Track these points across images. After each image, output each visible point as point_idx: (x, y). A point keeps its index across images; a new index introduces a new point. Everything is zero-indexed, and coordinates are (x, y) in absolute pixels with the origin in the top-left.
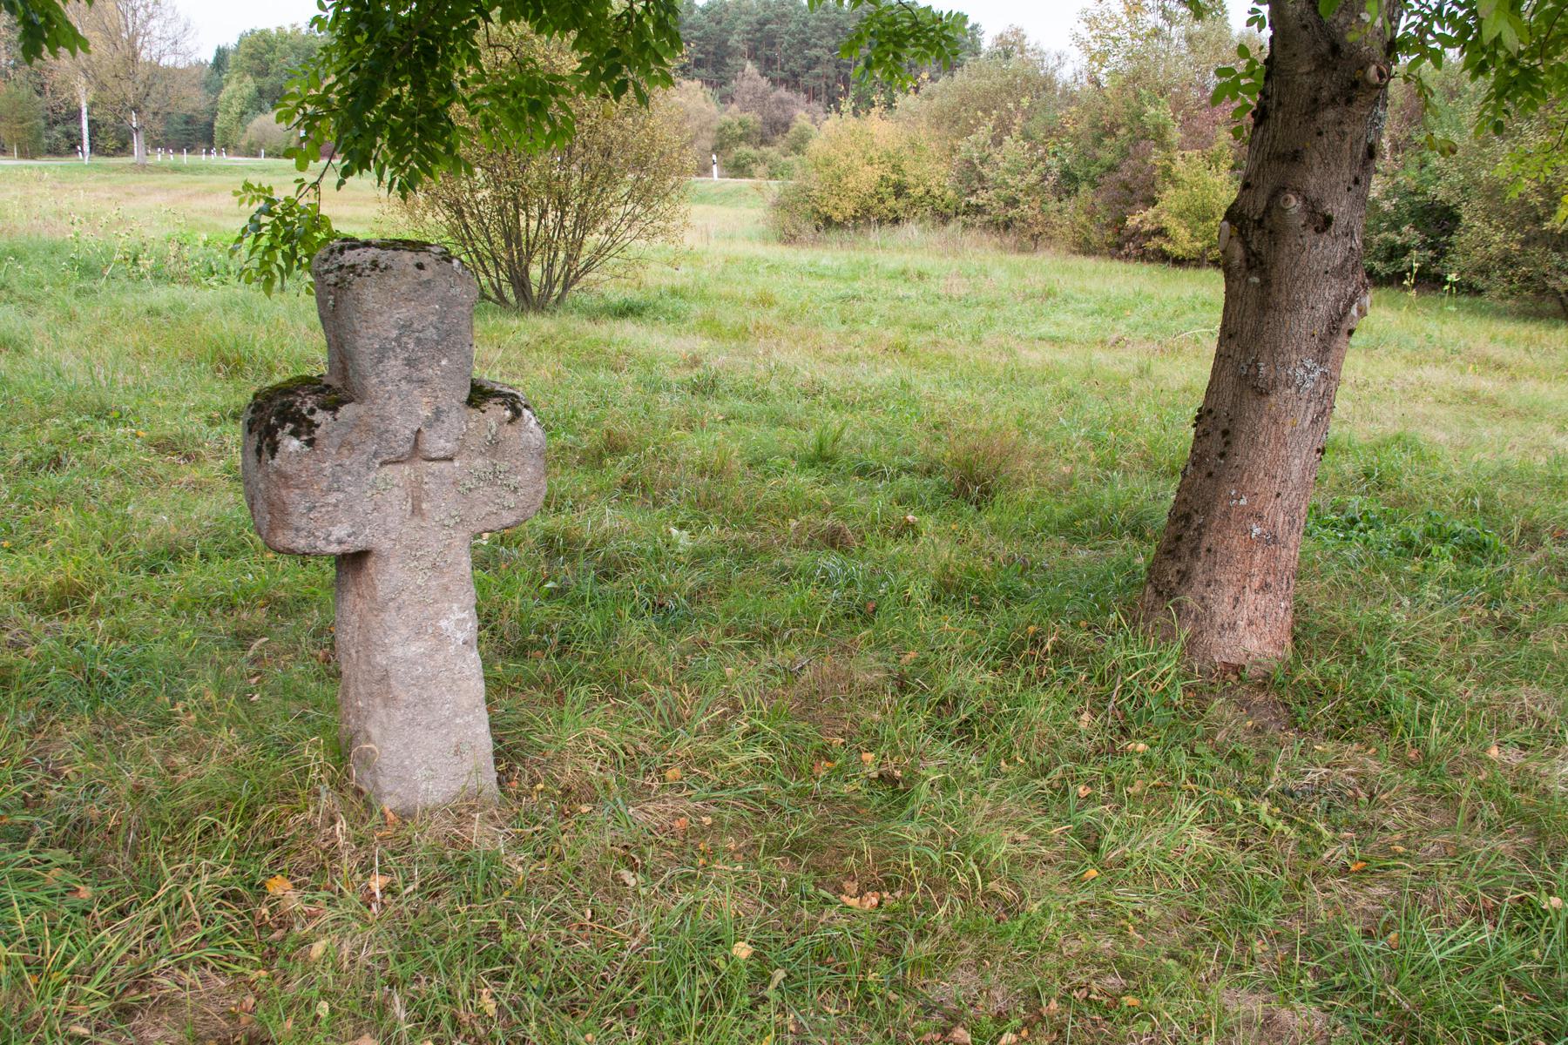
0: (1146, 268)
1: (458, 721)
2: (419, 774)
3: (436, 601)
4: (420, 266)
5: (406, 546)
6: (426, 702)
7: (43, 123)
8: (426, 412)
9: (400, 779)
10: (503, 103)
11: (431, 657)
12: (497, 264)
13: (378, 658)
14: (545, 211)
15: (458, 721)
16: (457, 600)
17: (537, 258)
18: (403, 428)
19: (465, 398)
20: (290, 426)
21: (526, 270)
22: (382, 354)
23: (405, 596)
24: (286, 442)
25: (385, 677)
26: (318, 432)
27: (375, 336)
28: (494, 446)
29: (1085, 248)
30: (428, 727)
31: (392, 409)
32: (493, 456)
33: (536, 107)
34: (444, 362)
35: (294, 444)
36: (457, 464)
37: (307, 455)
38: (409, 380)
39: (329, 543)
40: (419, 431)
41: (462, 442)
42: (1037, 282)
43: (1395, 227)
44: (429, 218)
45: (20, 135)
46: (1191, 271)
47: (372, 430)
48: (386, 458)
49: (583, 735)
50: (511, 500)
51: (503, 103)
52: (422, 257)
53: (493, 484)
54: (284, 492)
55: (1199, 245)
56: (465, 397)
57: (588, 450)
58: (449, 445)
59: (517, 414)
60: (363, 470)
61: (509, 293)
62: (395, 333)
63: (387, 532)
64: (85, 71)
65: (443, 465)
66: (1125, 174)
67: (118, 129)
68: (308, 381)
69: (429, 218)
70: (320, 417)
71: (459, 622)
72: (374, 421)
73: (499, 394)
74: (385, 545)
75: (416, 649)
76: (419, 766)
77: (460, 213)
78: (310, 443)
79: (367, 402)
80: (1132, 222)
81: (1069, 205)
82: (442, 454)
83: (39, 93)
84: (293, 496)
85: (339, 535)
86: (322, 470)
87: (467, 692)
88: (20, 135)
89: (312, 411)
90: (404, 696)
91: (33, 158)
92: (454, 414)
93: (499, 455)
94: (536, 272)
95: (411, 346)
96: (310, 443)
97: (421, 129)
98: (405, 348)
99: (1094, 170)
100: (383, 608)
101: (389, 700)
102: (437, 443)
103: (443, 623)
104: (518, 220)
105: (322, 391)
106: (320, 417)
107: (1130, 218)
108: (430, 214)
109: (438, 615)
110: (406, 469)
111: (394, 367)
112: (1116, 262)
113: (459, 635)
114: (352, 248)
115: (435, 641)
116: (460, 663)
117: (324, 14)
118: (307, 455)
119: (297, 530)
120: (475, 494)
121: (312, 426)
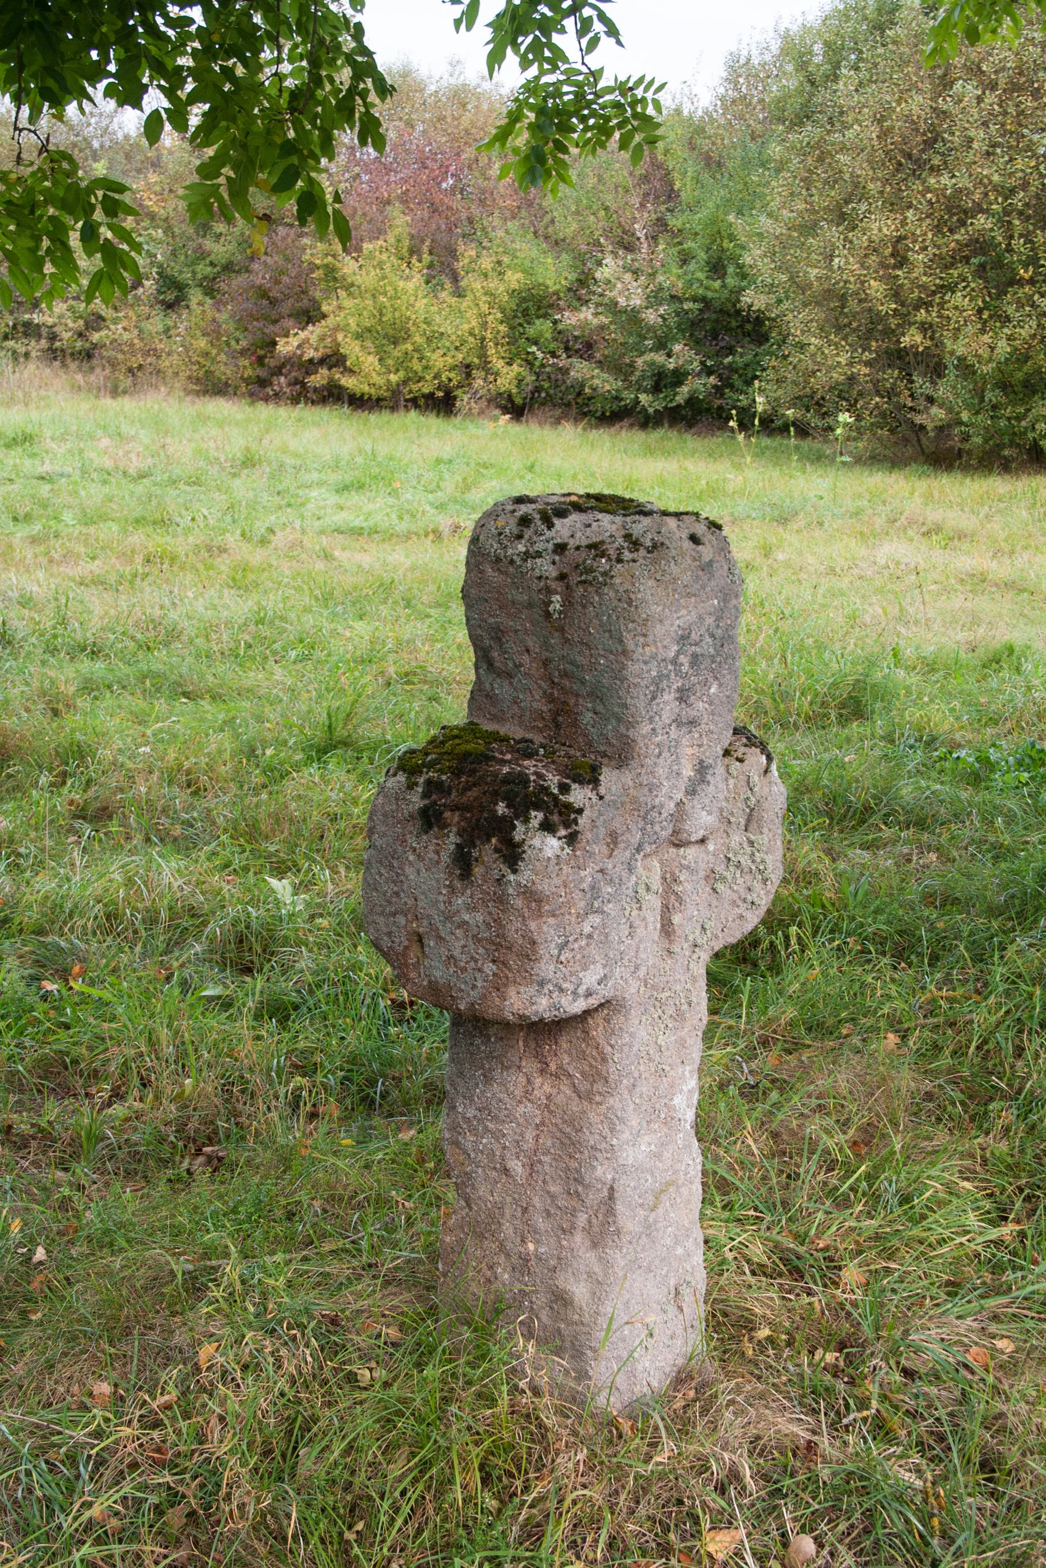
0: (305, 412)
13: (599, 1171)
20: (537, 817)
29: (211, 386)
35: (552, 845)
36: (711, 847)
42: (237, 443)
43: (662, 345)
46: (386, 416)
54: (533, 925)
55: (394, 378)
66: (260, 276)
70: (578, 795)
74: (633, 990)
78: (572, 839)
79: (633, 764)
80: (286, 347)
81: (182, 322)
89: (564, 789)
99: (203, 269)
106: (578, 795)
107: (281, 341)
112: (261, 406)
114: (561, 513)
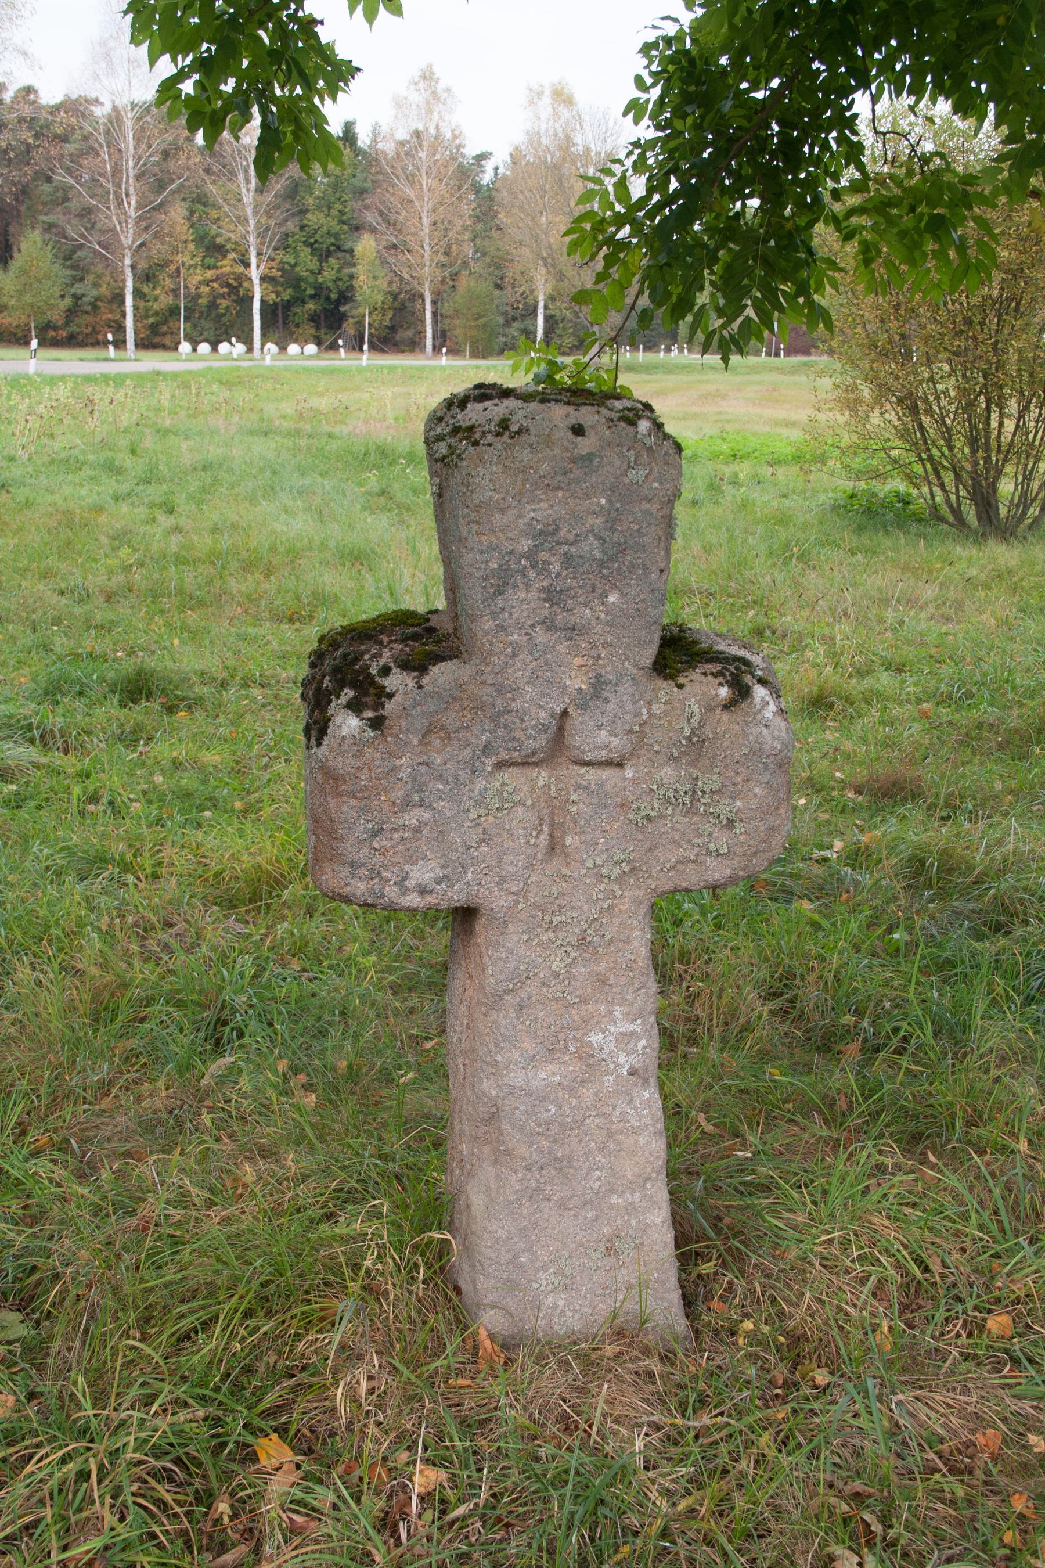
1: (614, 1199)
2: (544, 1280)
3: (585, 1001)
4: (578, 430)
5: (535, 905)
6: (562, 1165)
7: (501, 320)
8: (577, 683)
9: (511, 1286)
10: (891, 222)
11: (571, 1091)
12: (958, 477)
13: (485, 1084)
14: (1027, 408)
15: (614, 1199)
16: (623, 1002)
17: (1009, 469)
18: (536, 707)
19: (648, 662)
20: (348, 693)
21: (993, 487)
22: (503, 582)
23: (532, 987)
24: (338, 720)
25: (493, 1117)
26: (390, 706)
27: (492, 547)
28: (695, 747)
30: (562, 1205)
31: (518, 673)
32: (693, 763)
33: (938, 226)
34: (612, 598)
36: (629, 773)
37: (370, 743)
38: (550, 627)
39: (405, 891)
40: (565, 713)
41: (639, 735)
44: (875, 418)
45: (474, 333)
47: (482, 708)
48: (504, 755)
49: (851, 1229)
50: (722, 841)
51: (891, 222)
52: (587, 415)
53: (690, 811)
54: (332, 803)
56: (648, 655)
57: (1016, 731)
58: (615, 741)
59: (741, 692)
60: (464, 775)
61: (970, 514)
62: (525, 545)
63: (502, 881)
64: (544, 259)
65: (606, 773)
67: (576, 325)
68: (404, 618)
69: (875, 418)
70: (397, 681)
71: (624, 1034)
72: (485, 693)
73: (711, 656)
75: (546, 1075)
76: (544, 1268)
77: (914, 410)
79: (476, 660)
82: (603, 754)
83: (498, 286)
84: (348, 808)
85: (421, 879)
86: (395, 769)
87: (633, 1153)
88: (474, 333)
89: (386, 671)
90: (523, 1150)
91: (484, 358)
92: (626, 688)
93: (705, 762)
94: (1006, 488)
95: (555, 568)
96: (377, 723)
97: (767, 263)
98: (543, 569)
100: (495, 1002)
101: (502, 1156)
102: (594, 736)
103: (595, 1038)
104: (988, 418)
105: (415, 637)
106: (397, 681)
108: (877, 411)
109: (587, 1023)
110: (542, 776)
111: (524, 602)
113: (622, 1059)
115: (577, 1067)
116: (622, 1106)
117: (644, 96)
118: (370, 743)
119: (354, 865)
120: (660, 827)
121: (384, 695)
